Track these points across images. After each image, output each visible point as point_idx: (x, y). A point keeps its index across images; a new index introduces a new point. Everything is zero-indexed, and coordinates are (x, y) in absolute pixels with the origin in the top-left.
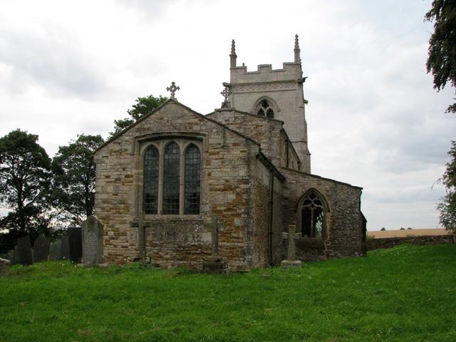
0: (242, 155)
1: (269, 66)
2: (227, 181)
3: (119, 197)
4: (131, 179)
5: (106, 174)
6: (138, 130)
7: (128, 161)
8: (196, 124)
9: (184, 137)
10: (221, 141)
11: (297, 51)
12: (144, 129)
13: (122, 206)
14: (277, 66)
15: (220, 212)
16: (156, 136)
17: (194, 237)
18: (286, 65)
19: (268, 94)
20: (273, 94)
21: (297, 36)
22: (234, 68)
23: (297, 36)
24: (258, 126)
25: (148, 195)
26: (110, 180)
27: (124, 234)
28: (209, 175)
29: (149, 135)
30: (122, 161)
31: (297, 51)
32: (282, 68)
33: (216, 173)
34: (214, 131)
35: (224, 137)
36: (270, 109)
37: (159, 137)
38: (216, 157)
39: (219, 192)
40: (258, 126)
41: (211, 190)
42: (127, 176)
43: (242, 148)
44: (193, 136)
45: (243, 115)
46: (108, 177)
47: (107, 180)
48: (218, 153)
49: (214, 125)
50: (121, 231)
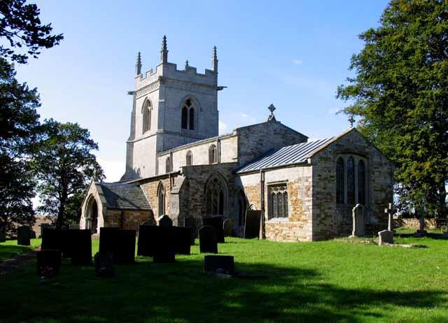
0: (389, 171)
1: (195, 69)
3: (327, 191)
4: (333, 179)
5: (318, 173)
7: (331, 166)
8: (367, 148)
11: (216, 61)
14: (201, 71)
15: (379, 204)
18: (207, 71)
25: (285, 185)
28: (374, 180)
30: (328, 166)
31: (216, 61)
32: (204, 73)
33: (377, 181)
35: (381, 158)
36: (192, 108)
41: (375, 190)
42: (331, 177)
43: (388, 166)
46: (319, 176)
48: (378, 168)
49: (376, 150)
50: (329, 214)
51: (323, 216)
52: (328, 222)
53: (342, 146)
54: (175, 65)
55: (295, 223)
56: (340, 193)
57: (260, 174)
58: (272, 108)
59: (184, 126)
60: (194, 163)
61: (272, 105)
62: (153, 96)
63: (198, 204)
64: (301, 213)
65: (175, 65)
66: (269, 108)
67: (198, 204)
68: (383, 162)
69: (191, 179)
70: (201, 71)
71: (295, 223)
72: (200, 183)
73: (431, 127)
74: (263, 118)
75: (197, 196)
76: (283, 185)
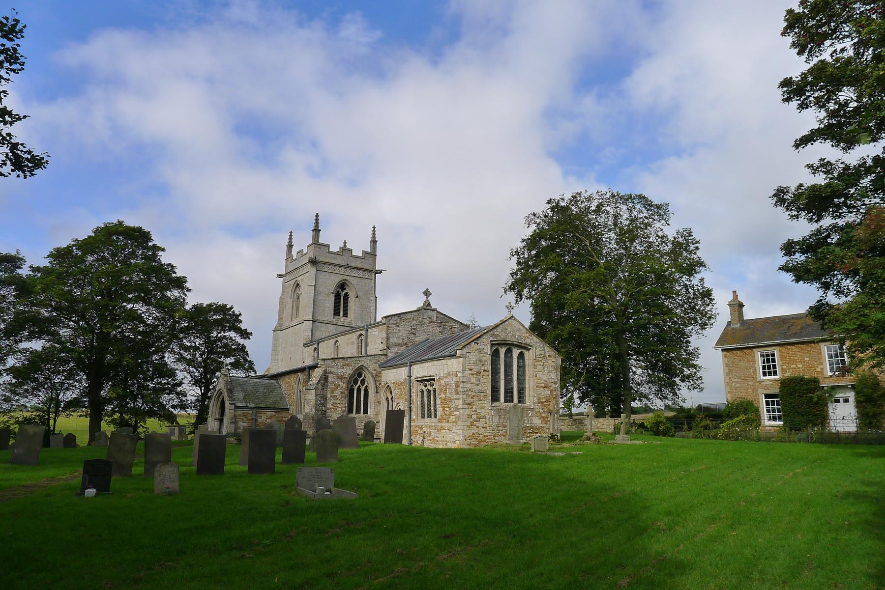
2: (546, 381)
4: (487, 373)
5: (470, 367)
6: (492, 335)
9: (519, 346)
10: (542, 353)
11: (374, 242)
12: (496, 336)
13: (482, 394)
15: (542, 403)
16: (504, 342)
17: (528, 420)
19: (348, 278)
20: (353, 279)
21: (374, 228)
22: (316, 243)
23: (374, 228)
24: (452, 327)
26: (473, 373)
27: (484, 417)
29: (500, 340)
31: (374, 242)
34: (538, 344)
36: (347, 293)
37: (503, 343)
38: (540, 363)
39: (541, 389)
40: (452, 327)
42: (485, 371)
44: (526, 346)
45: (442, 316)
46: (471, 370)
47: (470, 372)
51: (474, 416)
52: (481, 423)
53: (499, 335)
54: (329, 246)
55: (444, 425)
56: (495, 390)
57: (407, 368)
58: (427, 293)
59: (336, 313)
60: (749, 314)
61: (427, 289)
62: (302, 280)
63: (338, 402)
64: (450, 413)
65: (329, 246)
66: (430, 294)
67: (338, 402)
68: (547, 354)
69: (331, 373)
70: (357, 252)
71: (444, 425)
72: (342, 377)
73: (823, 195)
74: (416, 303)
75: (337, 393)
76: (431, 380)
